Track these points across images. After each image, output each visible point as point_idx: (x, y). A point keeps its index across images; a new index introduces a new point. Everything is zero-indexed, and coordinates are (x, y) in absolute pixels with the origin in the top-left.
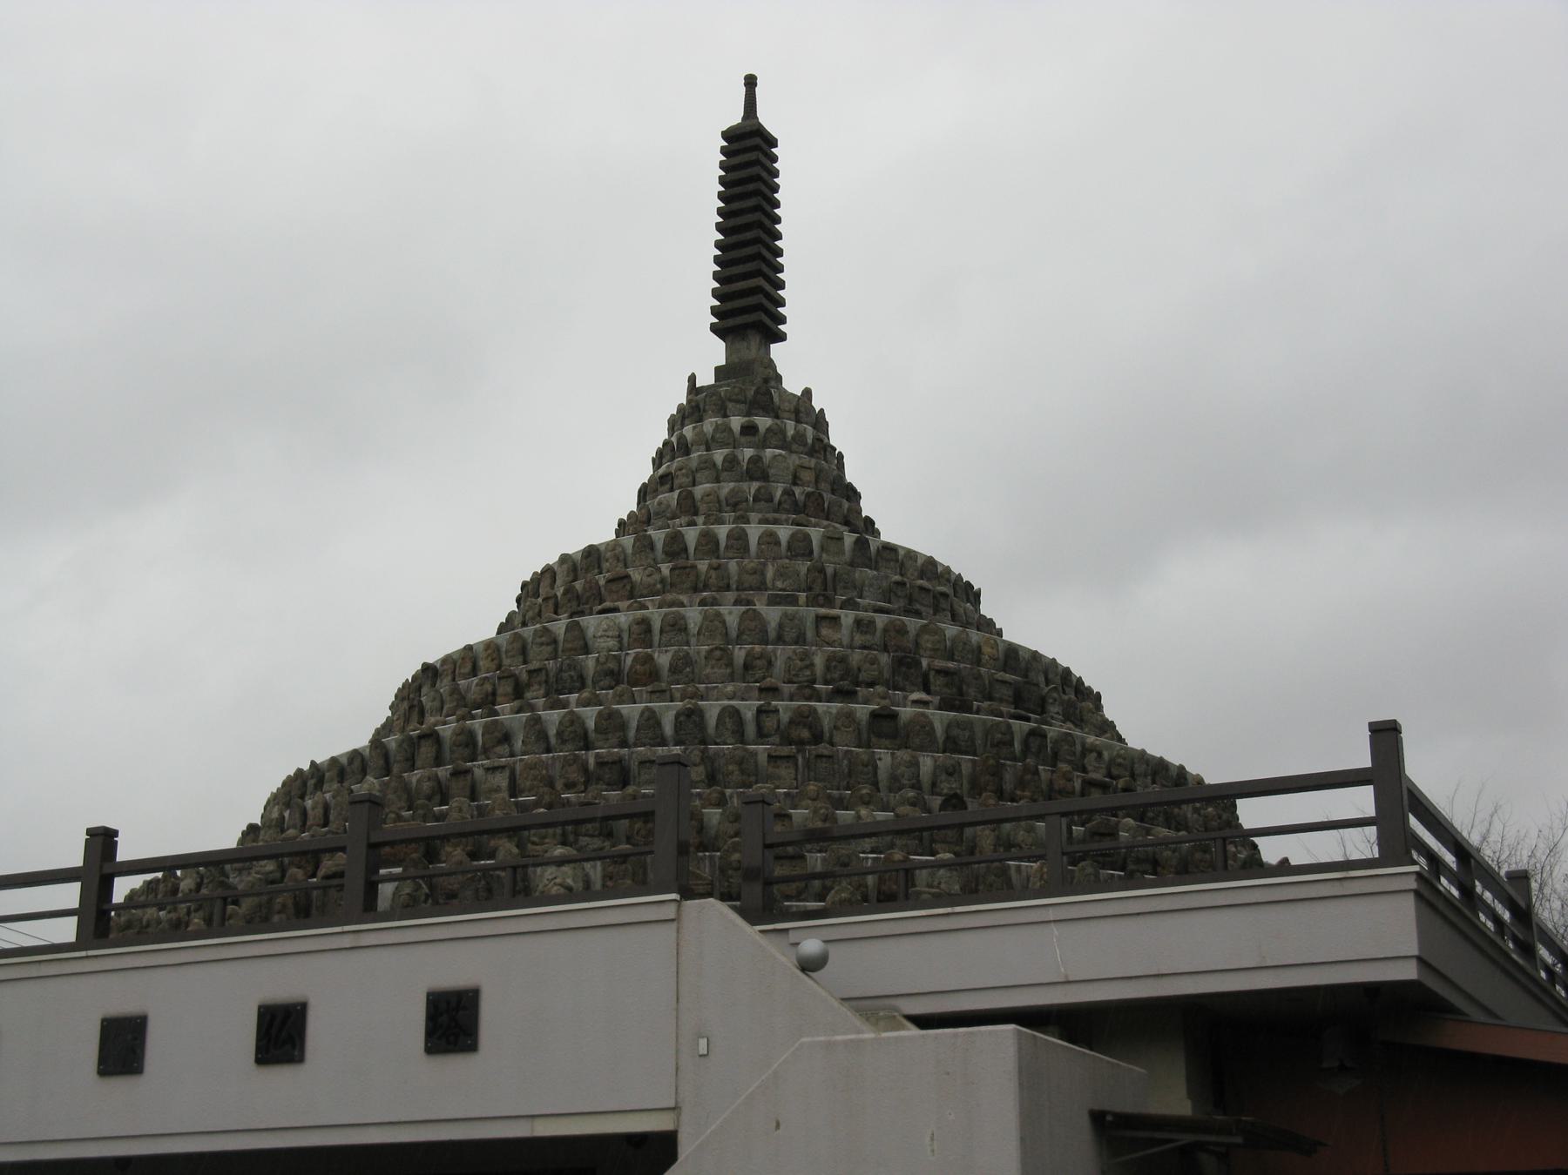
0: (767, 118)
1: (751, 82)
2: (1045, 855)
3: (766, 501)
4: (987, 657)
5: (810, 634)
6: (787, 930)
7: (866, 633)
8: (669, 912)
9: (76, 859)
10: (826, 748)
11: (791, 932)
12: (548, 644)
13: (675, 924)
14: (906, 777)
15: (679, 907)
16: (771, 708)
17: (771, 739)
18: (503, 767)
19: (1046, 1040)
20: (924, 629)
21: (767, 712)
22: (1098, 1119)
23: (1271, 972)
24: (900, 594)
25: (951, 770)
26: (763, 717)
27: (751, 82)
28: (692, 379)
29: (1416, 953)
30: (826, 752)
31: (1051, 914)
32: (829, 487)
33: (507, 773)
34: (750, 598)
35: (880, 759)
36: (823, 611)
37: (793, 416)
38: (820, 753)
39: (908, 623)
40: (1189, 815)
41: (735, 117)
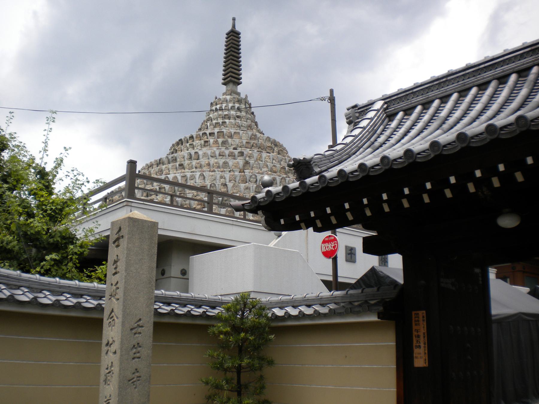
0: (238, 29)
1: (234, 19)
27: (234, 19)
41: (229, 28)
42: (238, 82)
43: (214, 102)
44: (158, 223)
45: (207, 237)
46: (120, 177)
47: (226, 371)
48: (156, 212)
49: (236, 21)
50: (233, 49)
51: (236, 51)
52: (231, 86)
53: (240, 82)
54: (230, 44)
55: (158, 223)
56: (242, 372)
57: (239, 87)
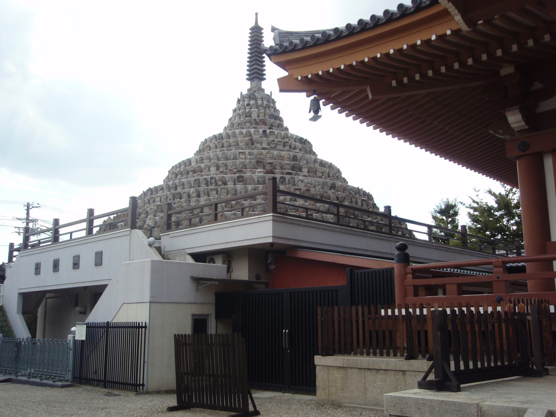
0: (260, 24)
1: (257, 14)
2: (488, 191)
3: (249, 122)
4: (286, 158)
5: (238, 156)
6: (169, 234)
7: (251, 155)
8: (128, 233)
9: (51, 226)
10: (223, 186)
11: (170, 235)
12: (184, 165)
13: (129, 236)
14: (243, 191)
15: (131, 232)
16: (213, 177)
17: (213, 185)
18: (159, 196)
19: (171, 262)
20: (267, 153)
21: (212, 178)
22: (192, 277)
23: (247, 240)
24: (273, 143)
25: (254, 189)
26: (212, 179)
27: (257, 14)
28: (241, 93)
29: (272, 235)
30: (223, 187)
31: (210, 229)
32: (269, 117)
33: (160, 197)
34: (231, 149)
35: (238, 188)
36: (241, 151)
37: (261, 100)
38: (184, 192)
39: (263, 152)
40: (331, 194)
41: (253, 24)
42: (261, 56)
43: (102, 232)
44: (277, 79)
45: (265, 222)
46: (281, 68)
47: (249, 98)
48: (267, 221)
49: (258, 16)
50: (257, 54)
51: (260, 59)
52: (256, 81)
53: (263, 65)
54: (253, 74)
55: (277, 79)
56: (48, 230)
57: (263, 82)
